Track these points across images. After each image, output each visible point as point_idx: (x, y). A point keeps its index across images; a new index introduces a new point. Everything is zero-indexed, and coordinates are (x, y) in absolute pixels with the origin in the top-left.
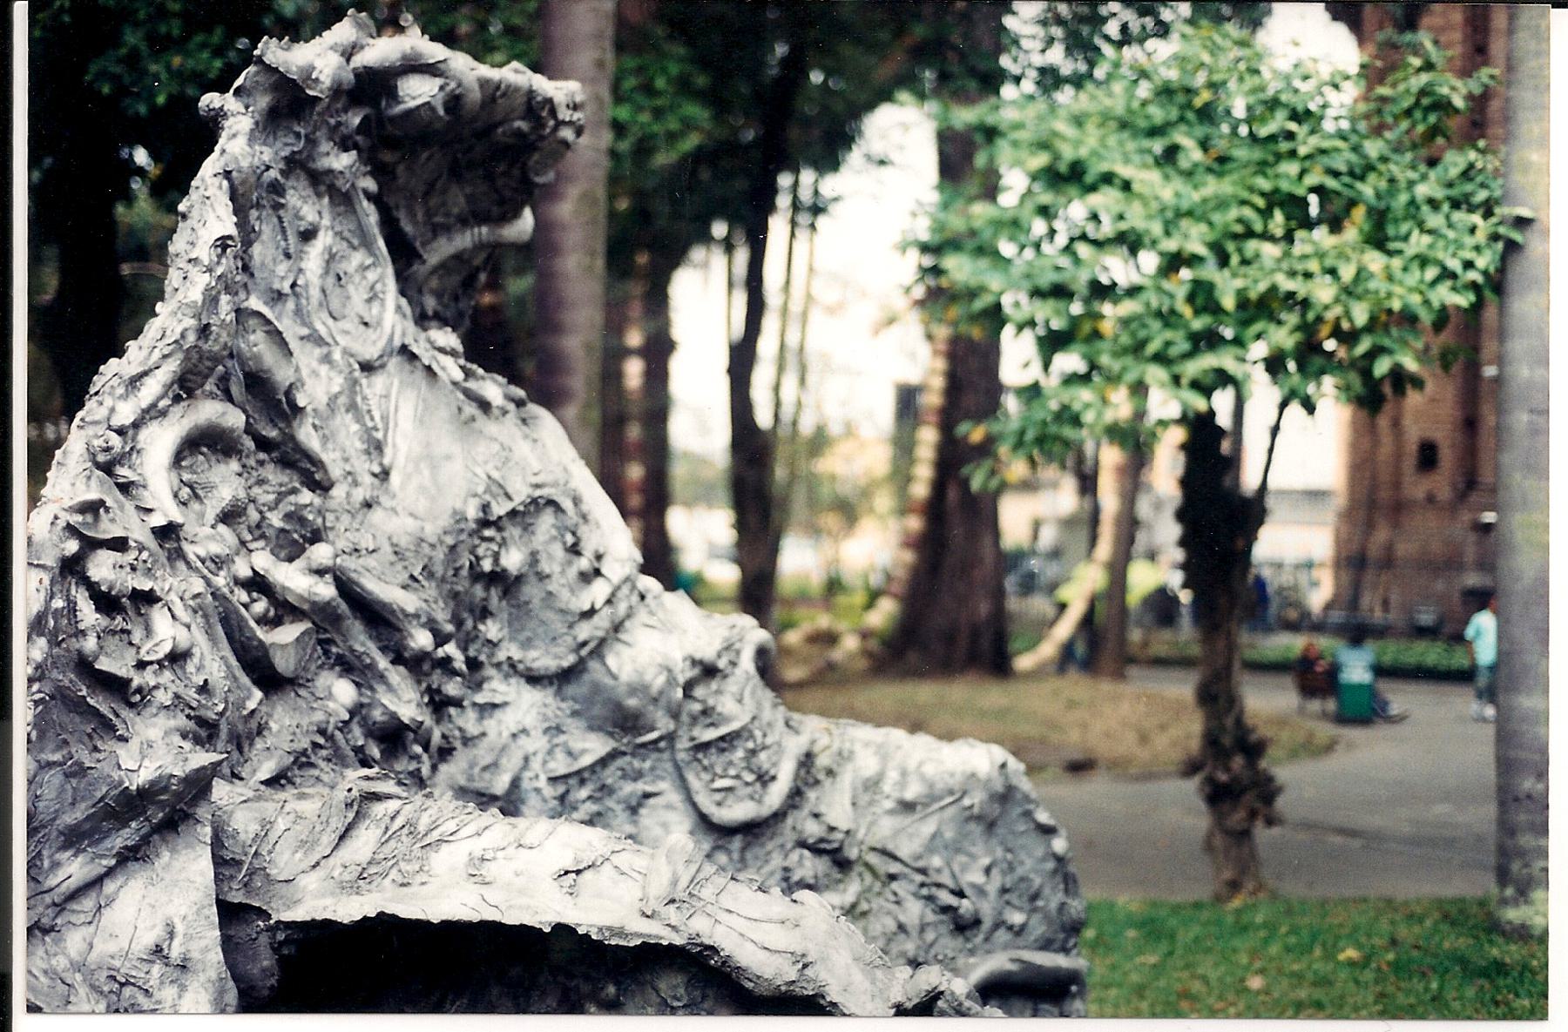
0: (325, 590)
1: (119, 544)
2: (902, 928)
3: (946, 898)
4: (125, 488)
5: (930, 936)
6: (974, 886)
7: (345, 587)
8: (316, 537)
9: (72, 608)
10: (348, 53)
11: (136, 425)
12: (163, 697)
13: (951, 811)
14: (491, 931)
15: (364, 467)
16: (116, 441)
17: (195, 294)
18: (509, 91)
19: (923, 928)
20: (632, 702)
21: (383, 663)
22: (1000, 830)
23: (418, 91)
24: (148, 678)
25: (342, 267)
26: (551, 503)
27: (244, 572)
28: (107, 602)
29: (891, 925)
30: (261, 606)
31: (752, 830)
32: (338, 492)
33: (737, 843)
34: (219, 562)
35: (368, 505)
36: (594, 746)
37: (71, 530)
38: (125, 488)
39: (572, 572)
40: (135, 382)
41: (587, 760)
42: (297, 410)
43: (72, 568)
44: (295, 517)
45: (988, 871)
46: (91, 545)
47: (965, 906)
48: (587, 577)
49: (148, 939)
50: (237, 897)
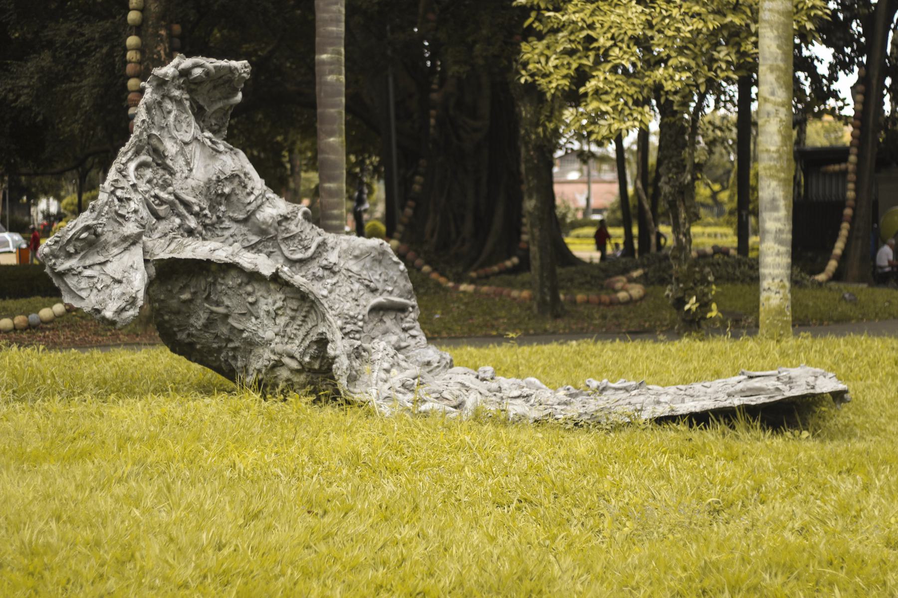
0: (172, 198)
1: (123, 188)
2: (352, 291)
3: (366, 282)
4: (124, 176)
5: (361, 293)
6: (376, 280)
7: (177, 197)
8: (170, 185)
9: (113, 201)
10: (176, 67)
11: (127, 162)
12: (133, 219)
13: (368, 259)
14: (194, 260)
15: (185, 169)
16: (122, 166)
17: (138, 133)
18: (224, 68)
19: (359, 291)
20: (264, 227)
21: (187, 214)
22: (383, 263)
23: (197, 72)
24: (130, 215)
25: (179, 118)
26: (237, 175)
27: (153, 194)
28: (120, 200)
29: (349, 289)
30: (157, 202)
31: (302, 262)
32: (178, 175)
33: (298, 265)
34: (146, 192)
35: (186, 178)
36: (255, 239)
37: (112, 185)
38: (124, 176)
39: (245, 193)
40: (126, 153)
41: (253, 243)
42: (166, 157)
43: (113, 193)
44: (165, 181)
45: (380, 275)
46: (116, 188)
47: (372, 285)
48: (249, 194)
49: (130, 264)
50: (148, 258)
